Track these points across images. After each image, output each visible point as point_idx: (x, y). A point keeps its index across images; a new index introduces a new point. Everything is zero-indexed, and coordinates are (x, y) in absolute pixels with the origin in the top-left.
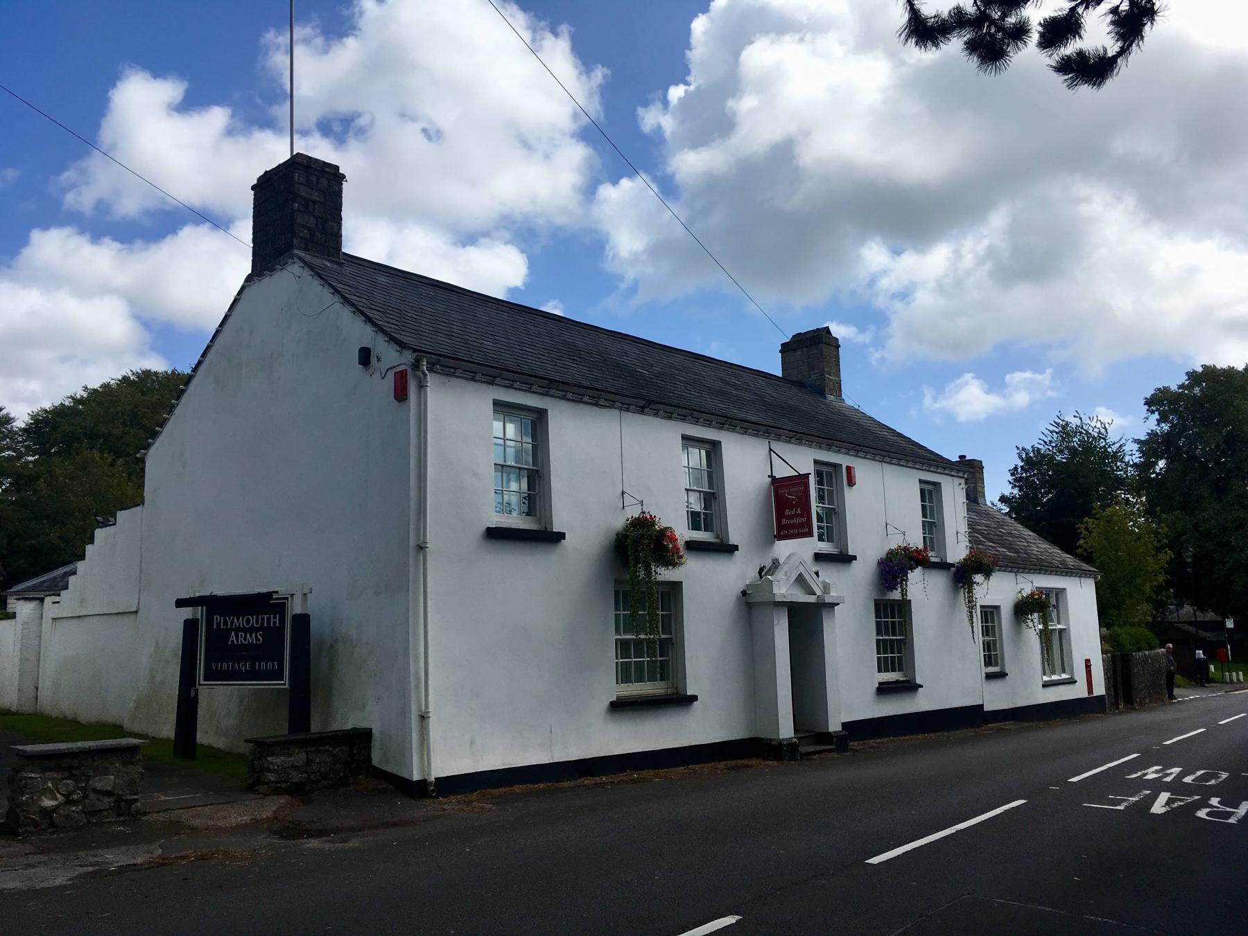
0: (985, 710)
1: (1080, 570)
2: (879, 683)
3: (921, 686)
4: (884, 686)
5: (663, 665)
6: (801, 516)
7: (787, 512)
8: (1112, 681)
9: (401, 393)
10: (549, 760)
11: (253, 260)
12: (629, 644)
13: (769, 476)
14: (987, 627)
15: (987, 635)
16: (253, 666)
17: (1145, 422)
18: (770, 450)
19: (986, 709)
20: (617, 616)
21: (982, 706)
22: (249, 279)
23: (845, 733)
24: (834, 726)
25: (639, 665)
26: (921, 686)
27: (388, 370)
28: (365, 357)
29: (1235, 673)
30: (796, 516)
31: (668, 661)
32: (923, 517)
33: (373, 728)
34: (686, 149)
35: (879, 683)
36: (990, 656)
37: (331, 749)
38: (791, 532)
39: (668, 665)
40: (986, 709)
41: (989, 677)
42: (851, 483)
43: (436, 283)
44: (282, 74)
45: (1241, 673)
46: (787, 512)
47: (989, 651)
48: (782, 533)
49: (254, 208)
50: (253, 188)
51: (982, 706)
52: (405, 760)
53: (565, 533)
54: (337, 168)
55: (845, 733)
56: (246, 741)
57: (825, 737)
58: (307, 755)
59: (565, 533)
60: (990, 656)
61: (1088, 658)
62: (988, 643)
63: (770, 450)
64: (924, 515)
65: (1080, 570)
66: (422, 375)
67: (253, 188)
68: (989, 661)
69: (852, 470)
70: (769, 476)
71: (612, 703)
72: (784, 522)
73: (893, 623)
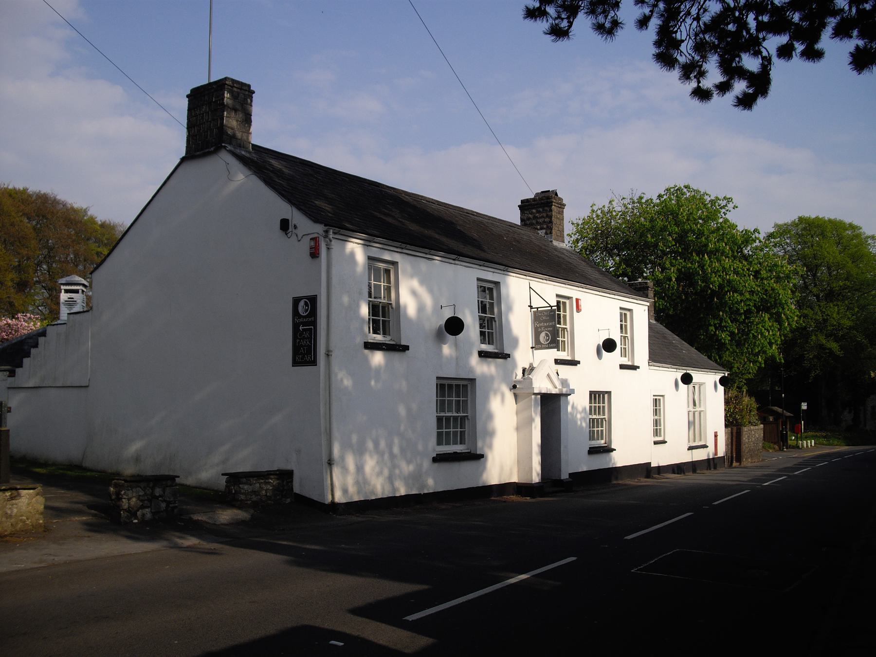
0: (652, 466)
1: (306, 212)
2: (590, 448)
3: (615, 450)
4: (592, 450)
5: (462, 434)
8: (730, 446)
9: (314, 254)
11: (186, 147)
12: (443, 419)
13: (529, 306)
14: (656, 410)
15: (656, 415)
18: (530, 288)
19: (652, 465)
20: (437, 400)
22: (183, 160)
23: (570, 480)
24: (565, 476)
25: (448, 433)
26: (615, 450)
27: (303, 236)
28: (285, 225)
29: (805, 442)
31: (465, 431)
32: (621, 333)
33: (294, 470)
35: (590, 448)
36: (657, 429)
37: (272, 482)
40: (652, 465)
41: (656, 443)
42: (578, 309)
43: (510, 224)
45: (813, 441)
47: (656, 426)
49: (188, 110)
50: (188, 96)
52: (323, 494)
54: (249, 86)
55: (570, 480)
56: (223, 475)
57: (559, 483)
58: (260, 484)
60: (657, 429)
61: (716, 431)
62: (656, 420)
63: (530, 288)
64: (622, 332)
65: (306, 212)
66: (329, 241)
67: (188, 96)
68: (656, 433)
69: (579, 301)
70: (529, 306)
71: (433, 458)
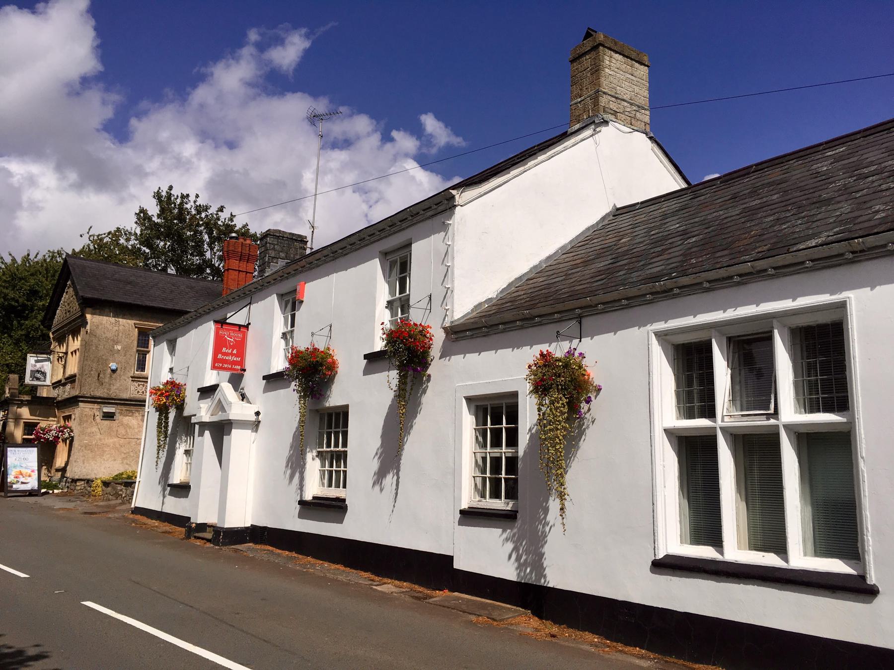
6: (236, 356)
7: (224, 350)
10: (19, 451)
16: (232, 366)
17: (381, 490)
19: (456, 566)
21: (451, 558)
30: (232, 354)
34: (188, 89)
38: (226, 366)
39: (493, 404)
40: (456, 566)
44: (733, 400)
46: (224, 350)
48: (216, 365)
51: (451, 558)
53: (364, 355)
59: (364, 355)
72: (220, 356)
73: (834, 367)
